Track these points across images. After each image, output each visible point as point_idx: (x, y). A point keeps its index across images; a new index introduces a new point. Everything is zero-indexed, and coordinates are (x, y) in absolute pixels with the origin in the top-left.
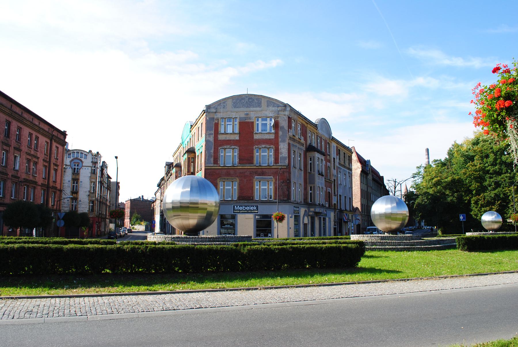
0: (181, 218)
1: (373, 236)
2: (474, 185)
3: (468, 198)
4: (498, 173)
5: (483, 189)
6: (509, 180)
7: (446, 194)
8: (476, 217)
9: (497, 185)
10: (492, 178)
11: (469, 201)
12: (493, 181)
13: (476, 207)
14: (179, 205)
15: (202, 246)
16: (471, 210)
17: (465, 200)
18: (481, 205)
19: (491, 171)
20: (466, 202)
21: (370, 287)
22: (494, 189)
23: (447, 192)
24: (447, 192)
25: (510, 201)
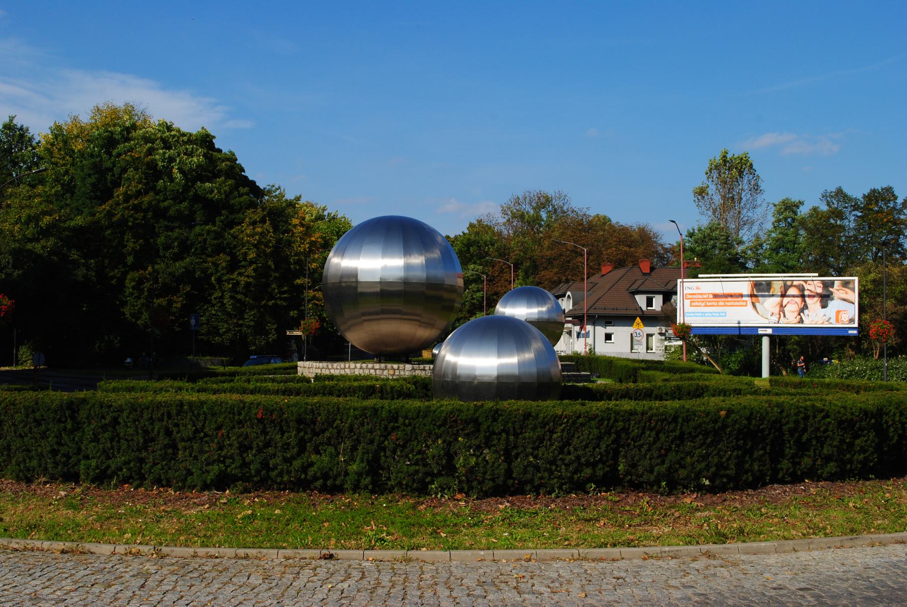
0: (418, 321)
1: (857, 393)
2: (131, 244)
3: (116, 272)
4: (188, 221)
5: (147, 255)
6: (215, 239)
7: (71, 258)
8: (134, 320)
9: (185, 248)
10: (172, 229)
11: (122, 280)
12: (176, 238)
13: (135, 297)
14: (401, 288)
15: (222, 396)
16: (124, 304)
17: (112, 278)
18: (150, 290)
19: (172, 212)
20: (114, 282)
21: (219, 525)
22: (177, 257)
23: (74, 255)
24: (74, 255)
25: (213, 287)
